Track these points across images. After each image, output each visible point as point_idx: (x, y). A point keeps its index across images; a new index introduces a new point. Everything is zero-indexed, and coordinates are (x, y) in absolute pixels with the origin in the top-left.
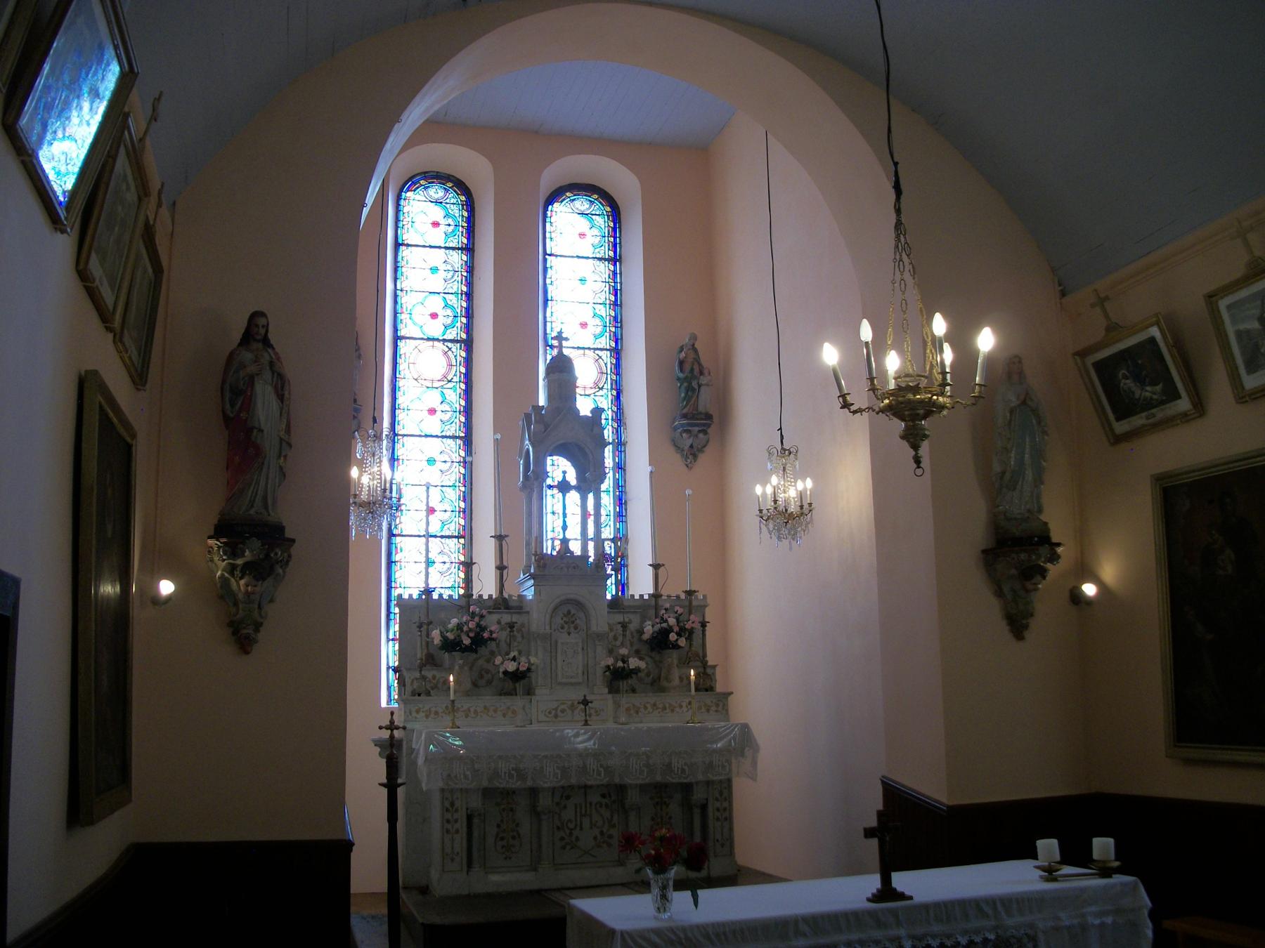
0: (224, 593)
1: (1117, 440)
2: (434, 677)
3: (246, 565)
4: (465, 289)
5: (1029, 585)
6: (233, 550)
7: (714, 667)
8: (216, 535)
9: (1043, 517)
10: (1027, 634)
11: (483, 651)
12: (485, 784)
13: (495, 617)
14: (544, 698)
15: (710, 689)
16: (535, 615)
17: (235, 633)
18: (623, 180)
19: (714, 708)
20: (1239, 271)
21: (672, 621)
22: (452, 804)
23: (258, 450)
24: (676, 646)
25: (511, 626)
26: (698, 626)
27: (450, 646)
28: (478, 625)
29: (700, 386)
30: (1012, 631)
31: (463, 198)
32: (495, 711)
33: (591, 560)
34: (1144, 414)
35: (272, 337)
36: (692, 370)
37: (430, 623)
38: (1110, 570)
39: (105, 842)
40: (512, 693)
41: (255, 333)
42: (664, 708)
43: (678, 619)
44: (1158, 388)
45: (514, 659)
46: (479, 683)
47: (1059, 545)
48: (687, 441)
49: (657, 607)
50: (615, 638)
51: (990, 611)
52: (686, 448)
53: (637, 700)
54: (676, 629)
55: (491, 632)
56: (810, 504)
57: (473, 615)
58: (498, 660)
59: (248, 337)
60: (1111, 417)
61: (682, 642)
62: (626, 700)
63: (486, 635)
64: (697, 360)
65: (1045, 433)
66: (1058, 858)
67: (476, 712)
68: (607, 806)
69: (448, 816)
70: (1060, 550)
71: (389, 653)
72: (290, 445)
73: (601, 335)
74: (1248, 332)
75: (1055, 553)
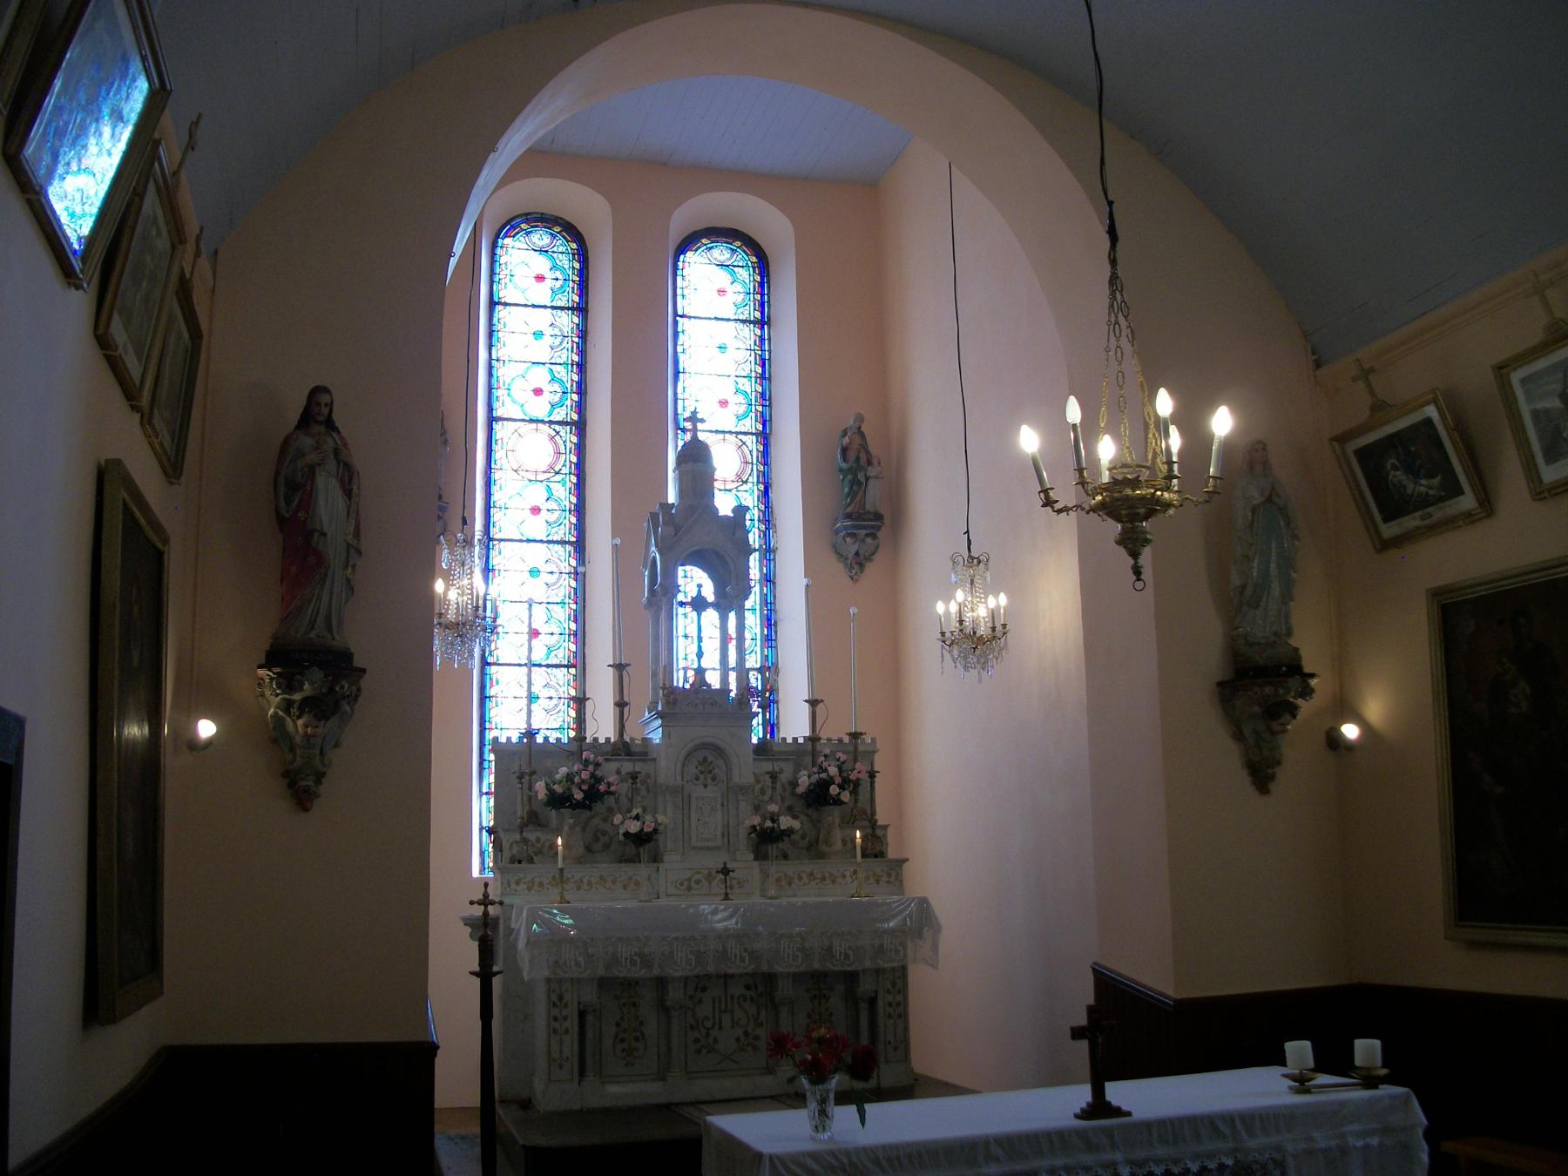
0: (278, 735)
1: (1385, 545)
2: (538, 840)
3: (305, 700)
4: (576, 358)
5: (1275, 726)
6: (288, 683)
7: (885, 827)
8: (268, 664)
9: (1293, 642)
10: (1272, 786)
11: (599, 807)
12: (601, 972)
13: (613, 766)
14: (674, 866)
15: (880, 855)
16: (663, 763)
17: (292, 785)
18: (772, 223)
19: (885, 879)
20: (1536, 337)
21: (833, 770)
22: (561, 998)
23: (320, 559)
24: (838, 802)
25: (634, 776)
26: (865, 777)
27: (558, 801)
28: (593, 776)
29: (867, 479)
30: (1254, 783)
31: (574, 246)
32: (614, 882)
33: (733, 694)
34: (1418, 514)
35: (337, 418)
36: (858, 459)
37: (533, 773)
38: (1376, 707)
39: (130, 1045)
40: (634, 860)
41: (316, 413)
42: (824, 879)
43: (840, 768)
44: (1436, 481)
45: (637, 818)
46: (593, 848)
47: (1312, 676)
48: (851, 547)
49: (814, 753)
50: (763, 792)
51: (1227, 758)
52: (851, 556)
53: (789, 868)
54: (838, 780)
55: (609, 784)
56: (1004, 626)
57: (586, 763)
58: (618, 819)
59: (307, 419)
60: (1378, 517)
61: (846, 796)
62: (776, 868)
63: (602, 788)
64: (864, 447)
65: (1295, 537)
66: (1311, 1064)
67: (590, 883)
68: (752, 999)
69: (556, 1012)
70: (1313, 682)
71: (482, 810)
72: (359, 552)
73: (745, 415)
74: (1547, 412)
75: (1308, 685)
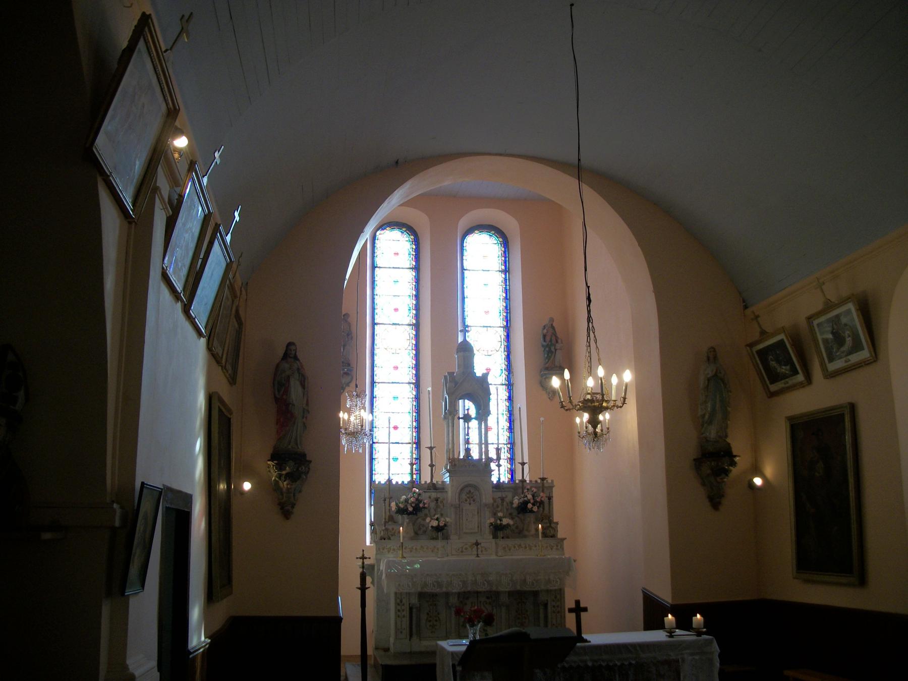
0: (276, 488)
1: (772, 395)
3: (287, 474)
6: (280, 467)
7: (557, 523)
8: (272, 459)
9: (728, 440)
11: (420, 514)
12: (419, 589)
13: (428, 494)
15: (553, 536)
16: (450, 494)
17: (282, 508)
18: (510, 223)
20: (820, 306)
21: (530, 497)
22: (401, 601)
24: (531, 511)
25: (437, 500)
26: (546, 500)
27: (401, 511)
28: (417, 499)
35: (300, 355)
37: (391, 498)
38: (769, 471)
39: (224, 609)
43: (533, 496)
44: (788, 367)
45: (437, 519)
46: (417, 533)
49: (523, 488)
50: (498, 507)
53: (510, 542)
54: (532, 501)
58: (428, 520)
59: (286, 356)
60: (768, 382)
61: (535, 509)
62: (501, 542)
64: (554, 334)
66: (674, 625)
68: (490, 603)
69: (399, 607)
70: (737, 459)
71: (369, 513)
72: (308, 412)
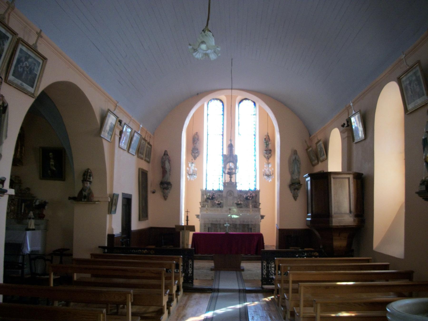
14: (225, 208)
18: (255, 98)
21: (249, 194)
23: (166, 171)
24: (249, 199)
25: (219, 195)
27: (208, 198)
35: (168, 154)
41: (166, 154)
46: (213, 205)
48: (267, 156)
59: (165, 154)
61: (250, 199)
